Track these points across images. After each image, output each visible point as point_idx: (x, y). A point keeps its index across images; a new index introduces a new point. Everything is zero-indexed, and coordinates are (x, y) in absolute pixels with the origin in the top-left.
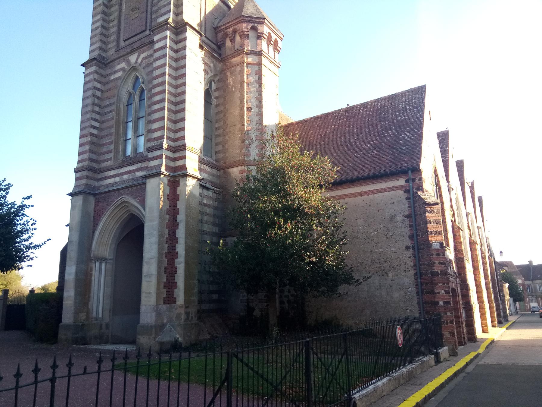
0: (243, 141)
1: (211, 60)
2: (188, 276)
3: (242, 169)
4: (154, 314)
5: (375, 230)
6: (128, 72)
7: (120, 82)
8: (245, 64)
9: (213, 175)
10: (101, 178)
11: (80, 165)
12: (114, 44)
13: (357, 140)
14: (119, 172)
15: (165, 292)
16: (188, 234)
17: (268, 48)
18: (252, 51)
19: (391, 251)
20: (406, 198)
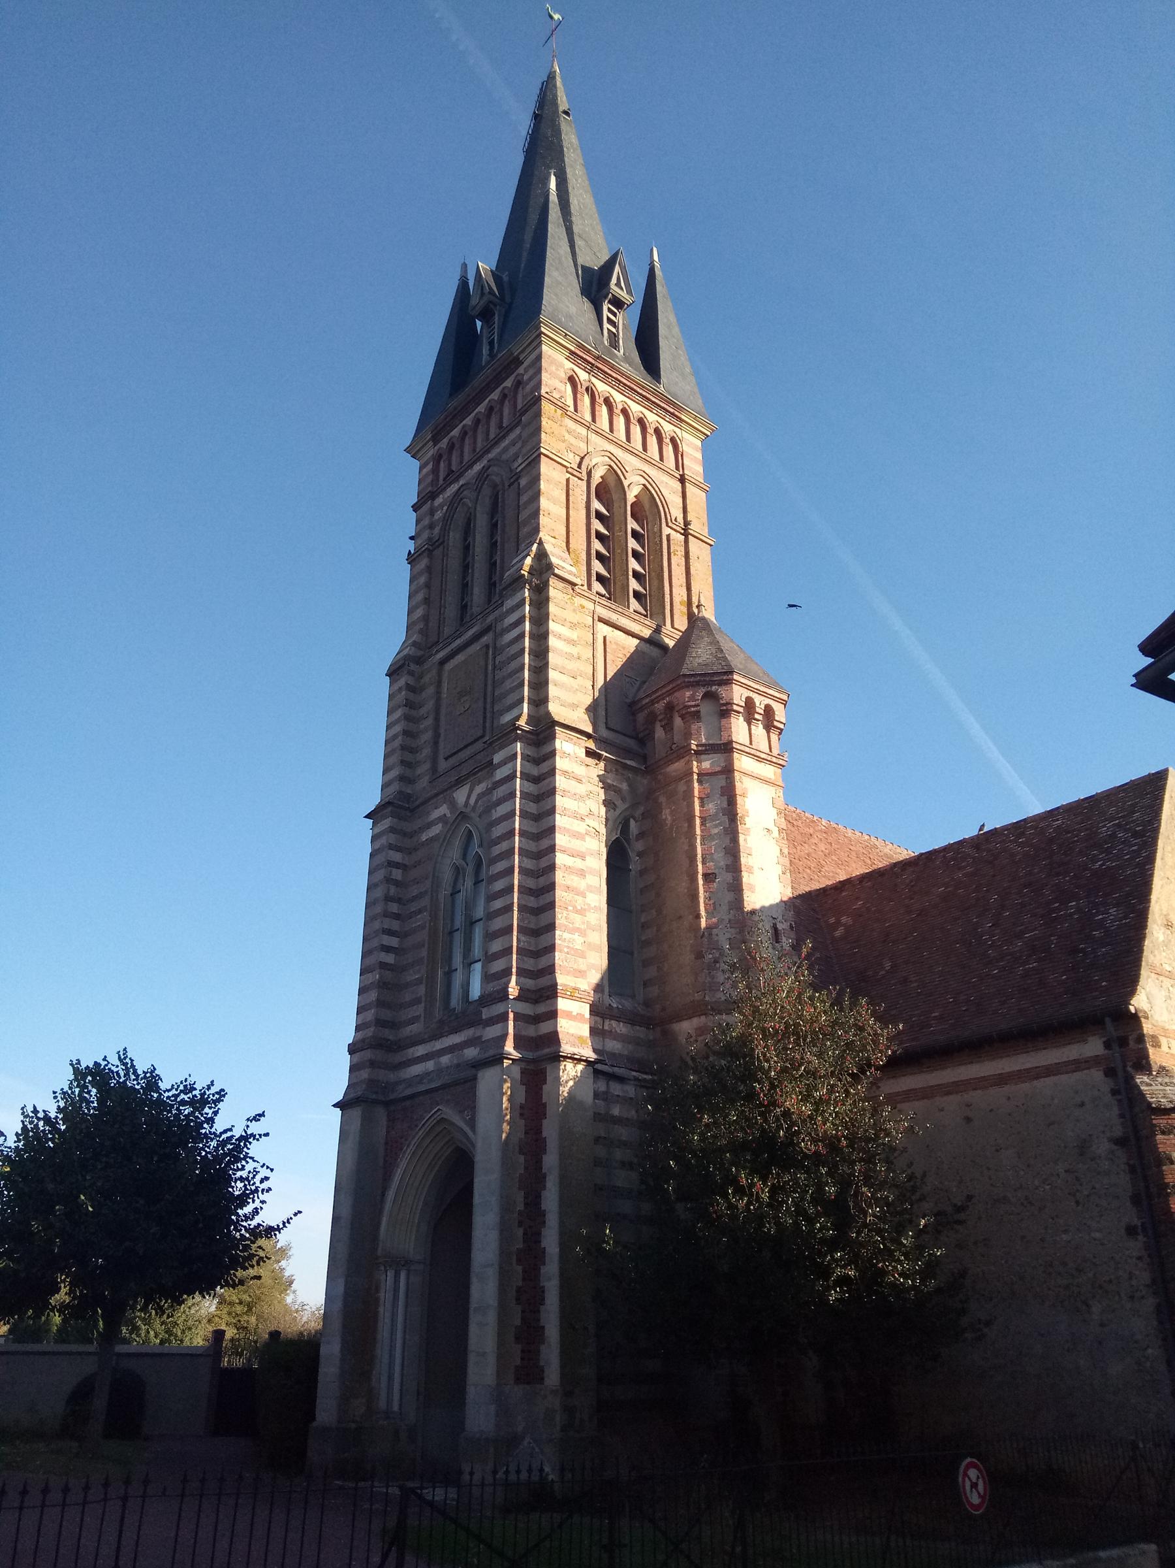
0: (699, 956)
1: (623, 774)
3: (702, 1025)
4: (493, 1408)
8: (695, 777)
9: (636, 1042)
12: (427, 766)
13: (993, 928)
14: (434, 1049)
16: (565, 1203)
17: (750, 730)
18: (709, 745)
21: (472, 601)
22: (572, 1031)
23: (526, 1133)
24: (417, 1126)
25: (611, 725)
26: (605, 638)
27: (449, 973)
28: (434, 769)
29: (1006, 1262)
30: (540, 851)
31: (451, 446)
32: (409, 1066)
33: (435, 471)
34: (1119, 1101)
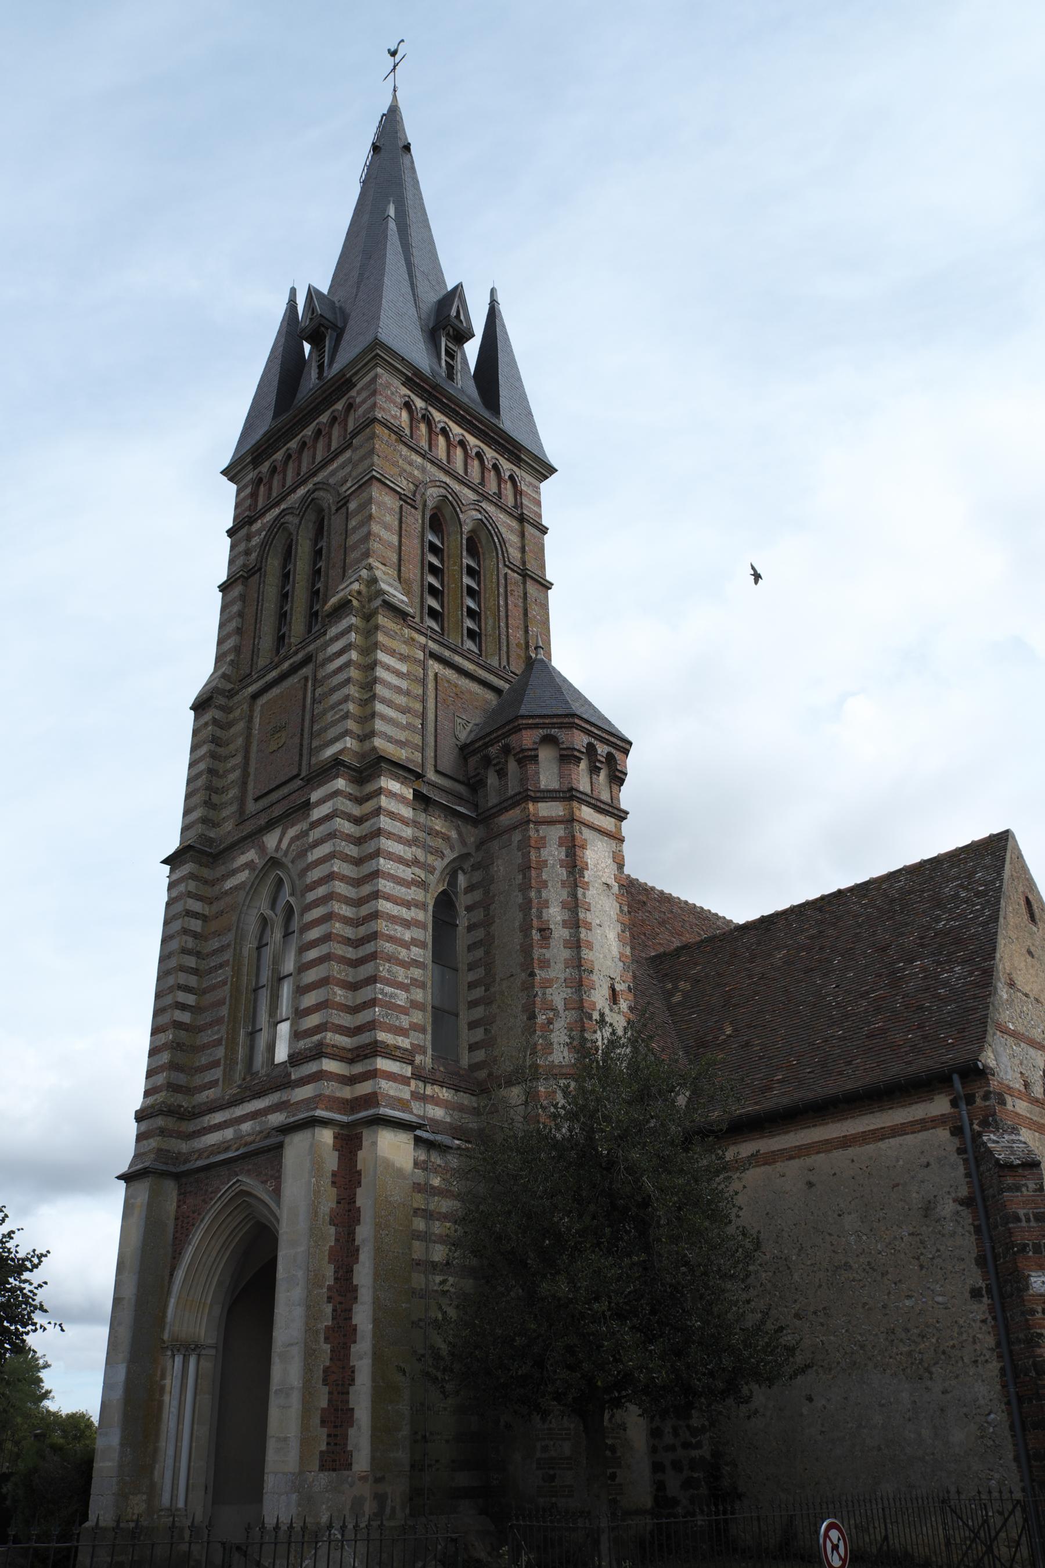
1: (452, 821)
2: (382, 1392)
5: (890, 1244)
6: (260, 871)
7: (242, 894)
9: (461, 1108)
10: (194, 1132)
11: (150, 1100)
12: (234, 808)
13: (837, 989)
14: (234, 1116)
15: (325, 1437)
19: (935, 1306)
20: (958, 1149)
21: (290, 631)
22: (392, 1093)
23: (338, 1202)
24: (211, 1199)
25: (440, 768)
26: (436, 674)
27: (253, 1034)
28: (242, 801)
29: (847, 1331)
30: (361, 898)
31: (273, 470)
32: (204, 1135)
33: (254, 495)
34: (965, 1161)
